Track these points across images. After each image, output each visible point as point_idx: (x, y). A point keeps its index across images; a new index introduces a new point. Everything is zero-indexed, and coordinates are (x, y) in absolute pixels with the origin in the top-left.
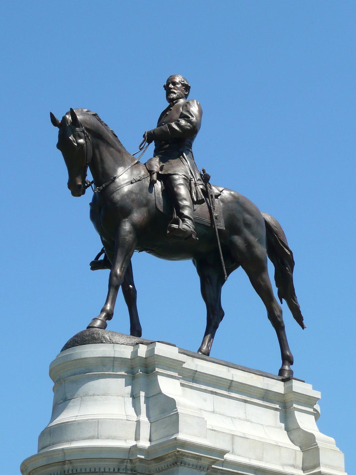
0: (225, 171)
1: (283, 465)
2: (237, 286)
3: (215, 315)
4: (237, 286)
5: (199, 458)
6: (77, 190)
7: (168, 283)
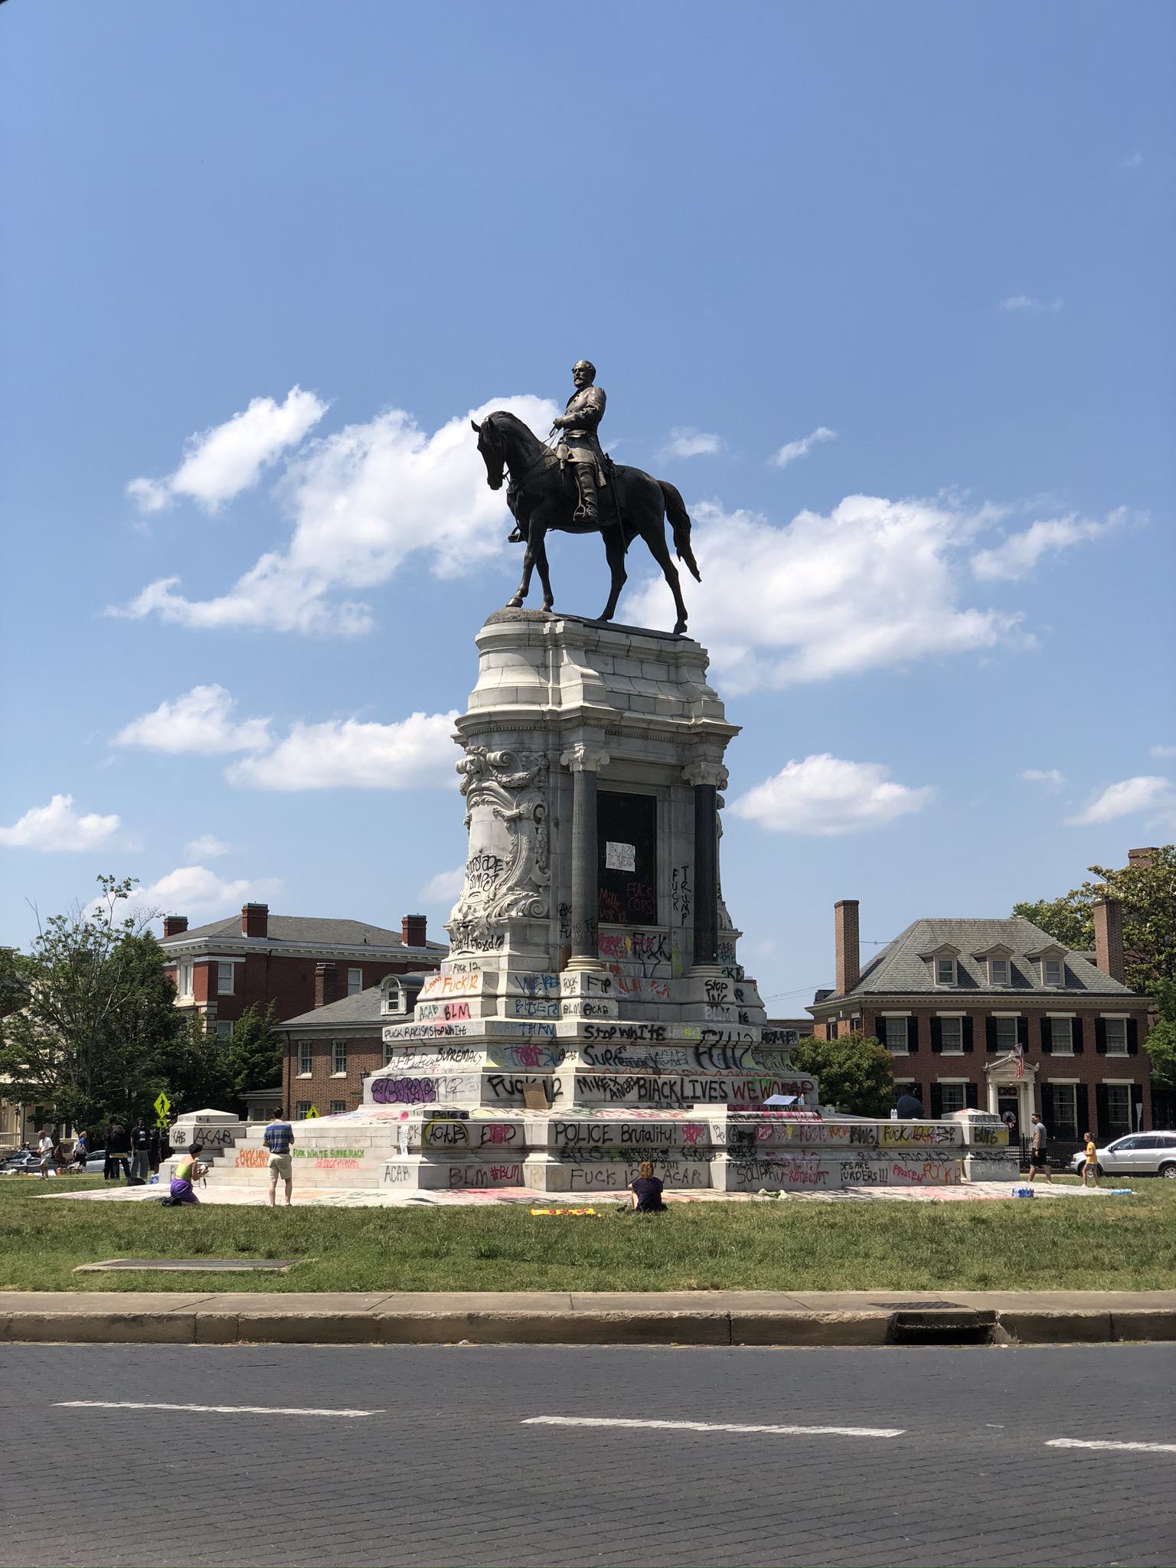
1: (672, 716)
2: (638, 549)
3: (619, 577)
4: (638, 549)
5: (599, 719)
6: (495, 482)
7: (576, 554)
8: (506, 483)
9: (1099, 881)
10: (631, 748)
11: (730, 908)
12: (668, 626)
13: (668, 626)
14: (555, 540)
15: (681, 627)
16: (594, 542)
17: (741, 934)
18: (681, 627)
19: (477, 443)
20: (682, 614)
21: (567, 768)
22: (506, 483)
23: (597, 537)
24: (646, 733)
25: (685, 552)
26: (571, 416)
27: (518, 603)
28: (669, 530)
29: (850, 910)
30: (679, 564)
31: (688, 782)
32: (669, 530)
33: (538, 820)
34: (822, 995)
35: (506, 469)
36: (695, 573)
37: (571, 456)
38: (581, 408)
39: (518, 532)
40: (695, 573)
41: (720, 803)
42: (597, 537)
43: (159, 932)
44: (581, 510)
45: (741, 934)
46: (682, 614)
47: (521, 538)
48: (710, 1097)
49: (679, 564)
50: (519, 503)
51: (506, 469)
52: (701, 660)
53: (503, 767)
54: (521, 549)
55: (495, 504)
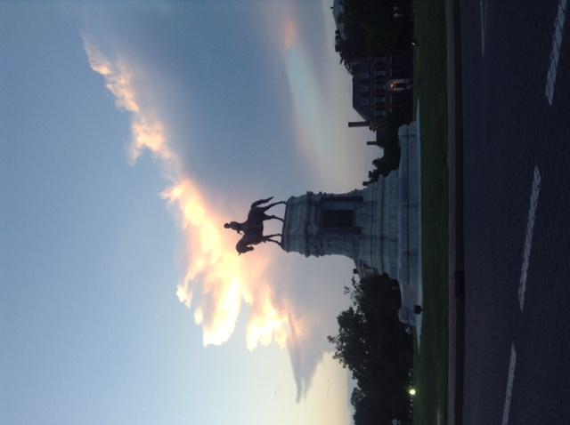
2: (268, 213)
3: (273, 217)
4: (268, 213)
6: (252, 249)
9: (343, 63)
10: (312, 218)
11: (349, 259)
12: (285, 205)
13: (285, 205)
14: (265, 233)
15: (284, 203)
16: (265, 223)
18: (284, 203)
20: (281, 202)
24: (309, 215)
28: (262, 205)
29: (351, 124)
32: (262, 205)
34: (371, 129)
36: (270, 199)
40: (270, 199)
41: (325, 194)
43: (349, 294)
46: (281, 202)
50: (257, 241)
52: (293, 198)
53: (316, 247)
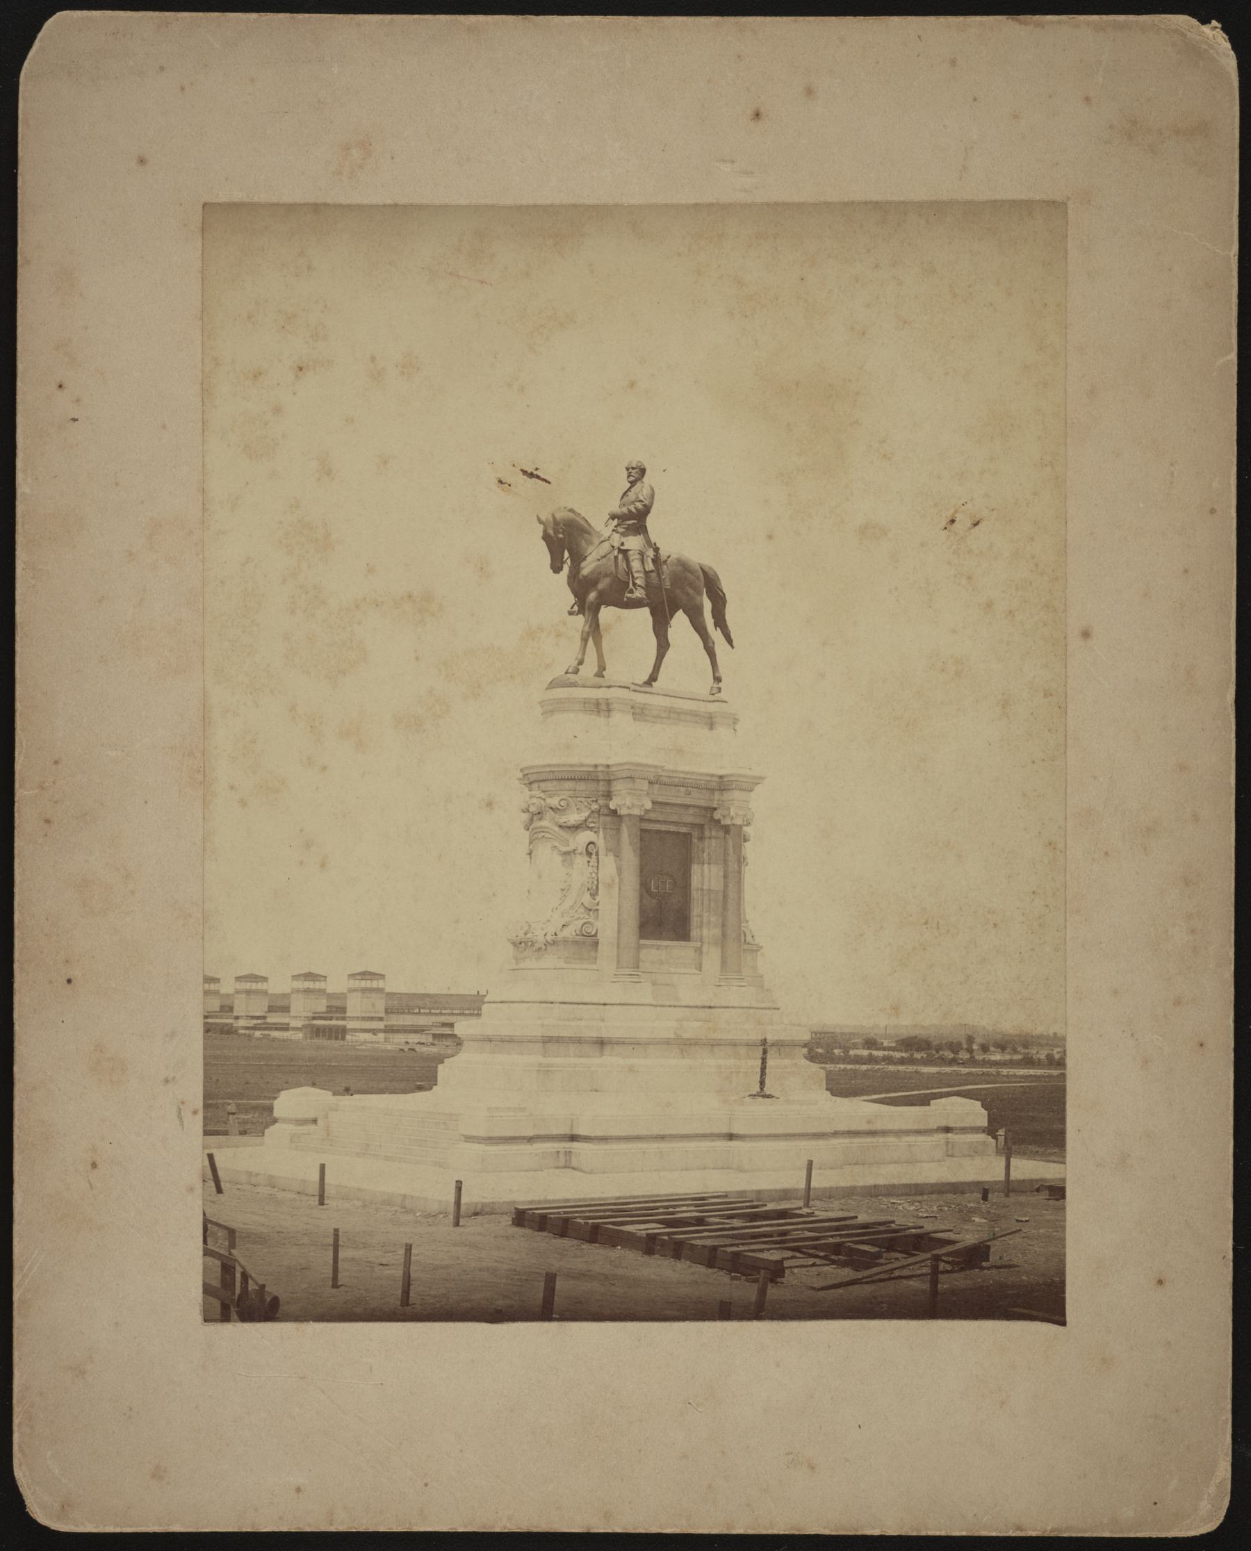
0: (676, 536)
3: (663, 646)
4: (680, 623)
6: (556, 568)
7: (630, 627)
8: (566, 568)
14: (607, 614)
15: (805, 1046)
17: (1063, 1323)
19: (541, 534)
21: (615, 812)
22: (566, 568)
23: (645, 612)
25: (720, 622)
26: (625, 510)
27: (576, 672)
28: (707, 606)
30: (716, 635)
31: (719, 821)
33: (589, 854)
35: (566, 554)
37: (622, 544)
38: (633, 503)
39: (576, 608)
42: (645, 612)
44: (631, 592)
45: (1063, 1323)
47: (579, 613)
48: (259, 1039)
49: (716, 635)
51: (566, 554)
54: (580, 621)
55: (557, 590)
